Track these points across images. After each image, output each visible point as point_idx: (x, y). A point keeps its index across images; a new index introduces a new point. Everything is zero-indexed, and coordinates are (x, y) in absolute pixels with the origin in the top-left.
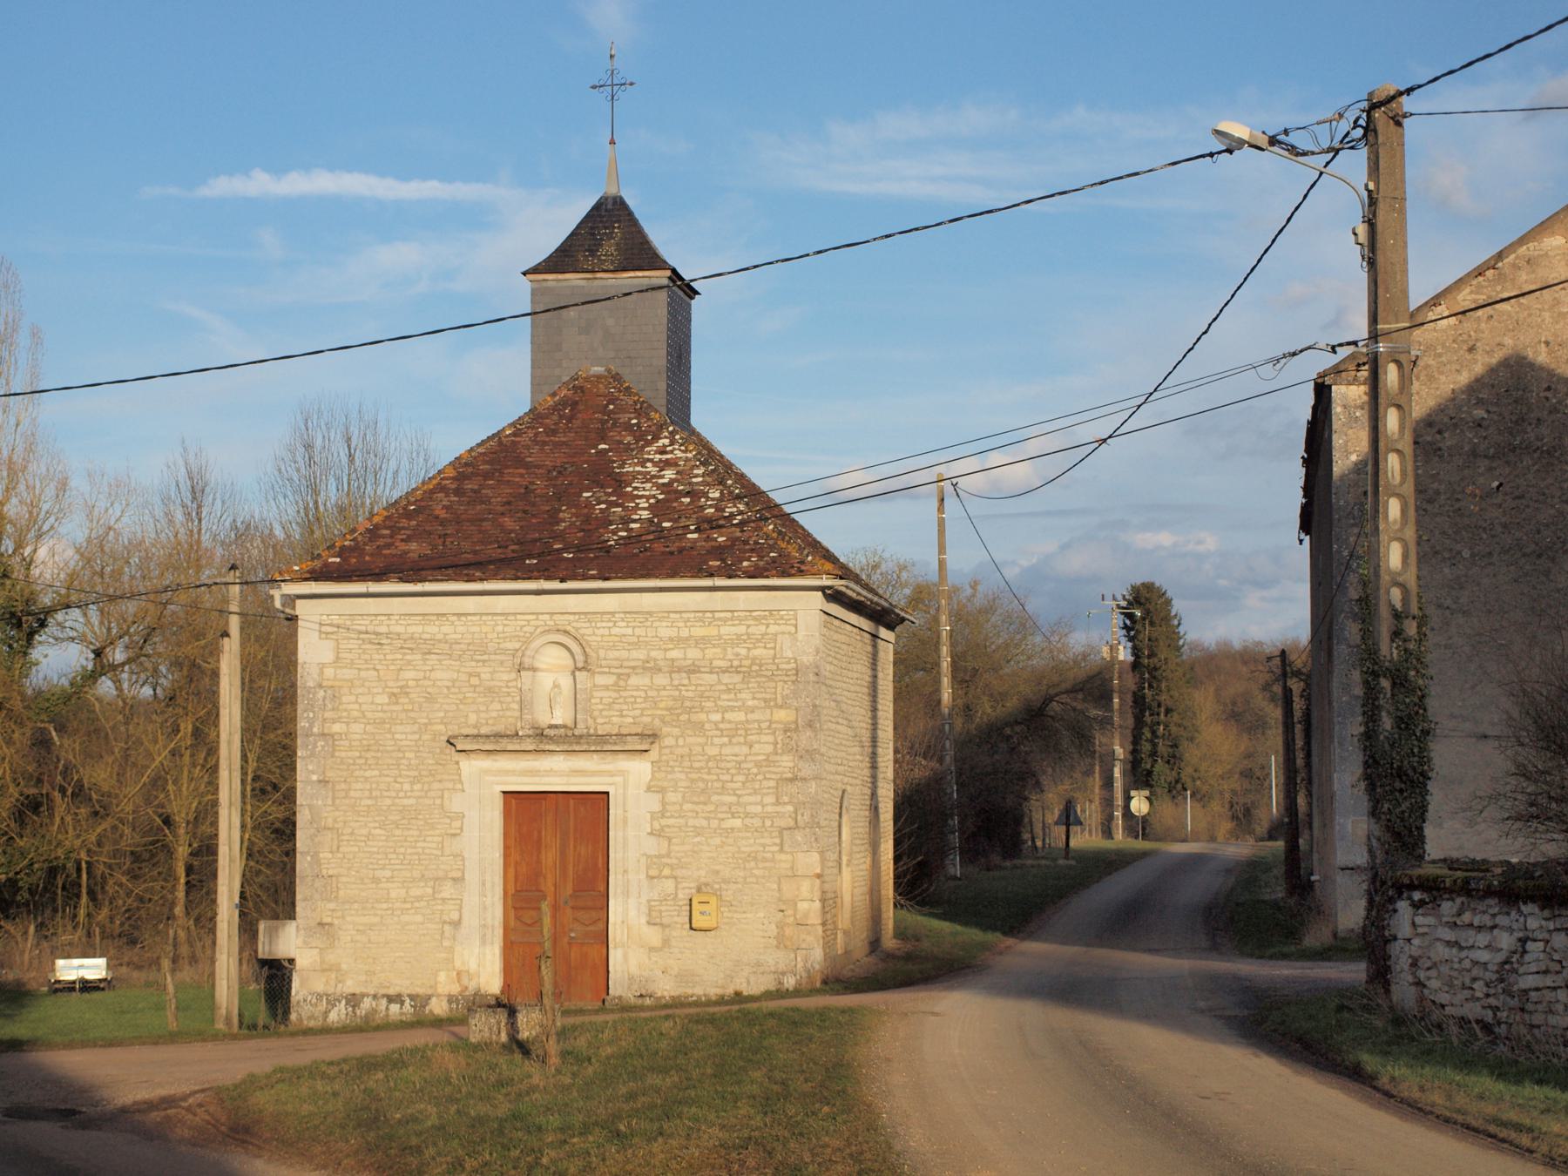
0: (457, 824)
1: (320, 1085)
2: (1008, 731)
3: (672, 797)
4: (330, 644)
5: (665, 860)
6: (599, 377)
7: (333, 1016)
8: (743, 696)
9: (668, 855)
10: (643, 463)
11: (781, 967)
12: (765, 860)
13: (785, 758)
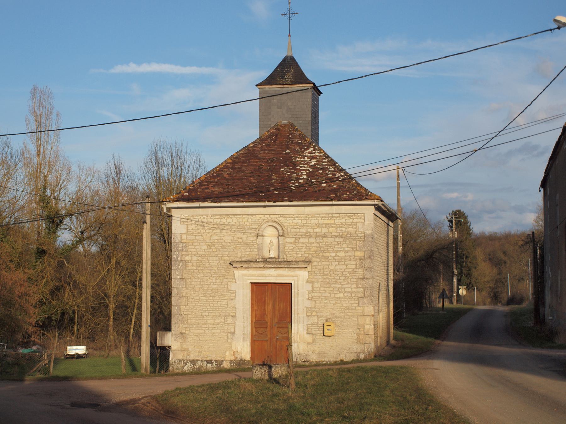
0: (233, 295)
1: (198, 396)
2: (418, 263)
3: (316, 285)
4: (185, 226)
5: (313, 309)
6: (285, 125)
7: (186, 368)
8: (343, 246)
9: (315, 307)
10: (304, 157)
11: (359, 351)
12: (352, 309)
13: (360, 270)
